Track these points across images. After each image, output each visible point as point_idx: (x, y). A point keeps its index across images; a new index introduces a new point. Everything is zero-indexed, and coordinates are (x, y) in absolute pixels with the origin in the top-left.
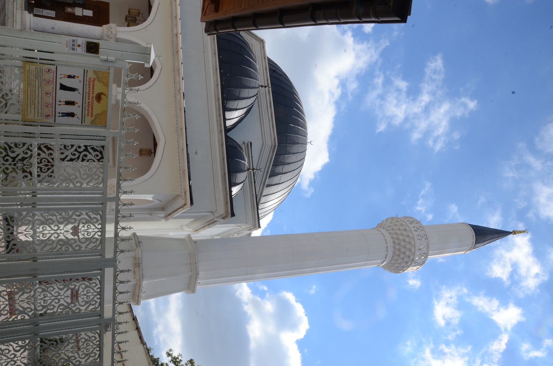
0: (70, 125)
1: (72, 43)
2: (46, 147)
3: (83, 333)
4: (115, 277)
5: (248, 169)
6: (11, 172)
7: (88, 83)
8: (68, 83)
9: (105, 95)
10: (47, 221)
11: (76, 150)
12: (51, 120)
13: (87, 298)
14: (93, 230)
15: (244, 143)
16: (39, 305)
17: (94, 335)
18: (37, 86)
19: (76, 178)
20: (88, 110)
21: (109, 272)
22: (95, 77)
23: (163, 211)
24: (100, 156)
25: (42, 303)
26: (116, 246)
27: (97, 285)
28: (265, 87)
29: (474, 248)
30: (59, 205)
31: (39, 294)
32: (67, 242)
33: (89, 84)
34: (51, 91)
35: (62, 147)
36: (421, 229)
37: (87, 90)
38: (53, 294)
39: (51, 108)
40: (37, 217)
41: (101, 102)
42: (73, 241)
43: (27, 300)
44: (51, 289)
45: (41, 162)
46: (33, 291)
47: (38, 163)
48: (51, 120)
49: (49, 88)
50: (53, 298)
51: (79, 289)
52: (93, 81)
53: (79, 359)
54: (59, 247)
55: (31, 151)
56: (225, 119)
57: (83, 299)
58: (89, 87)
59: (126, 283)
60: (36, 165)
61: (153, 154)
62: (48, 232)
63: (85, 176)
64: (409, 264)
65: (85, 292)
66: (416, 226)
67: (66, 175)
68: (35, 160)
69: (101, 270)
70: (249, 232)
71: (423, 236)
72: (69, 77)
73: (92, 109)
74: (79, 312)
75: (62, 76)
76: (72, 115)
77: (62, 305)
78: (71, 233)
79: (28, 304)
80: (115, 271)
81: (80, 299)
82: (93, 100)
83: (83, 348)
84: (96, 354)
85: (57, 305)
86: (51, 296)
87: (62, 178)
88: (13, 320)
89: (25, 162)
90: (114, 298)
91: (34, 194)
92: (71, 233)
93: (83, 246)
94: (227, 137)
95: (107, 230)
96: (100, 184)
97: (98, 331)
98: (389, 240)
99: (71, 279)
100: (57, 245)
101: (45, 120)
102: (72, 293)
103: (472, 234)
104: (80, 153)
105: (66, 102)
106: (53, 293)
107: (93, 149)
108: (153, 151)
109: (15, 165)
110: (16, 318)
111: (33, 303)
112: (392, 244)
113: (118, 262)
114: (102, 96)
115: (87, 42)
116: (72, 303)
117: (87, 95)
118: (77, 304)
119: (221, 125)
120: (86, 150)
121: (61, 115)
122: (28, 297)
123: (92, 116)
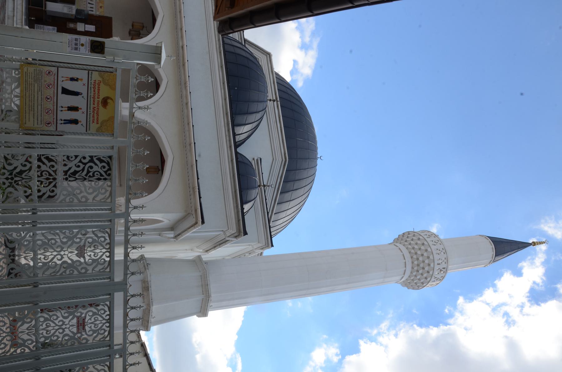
0: (74, 134)
1: (74, 42)
2: (47, 158)
3: (91, 366)
4: (126, 302)
5: (259, 186)
6: (9, 186)
7: (92, 86)
8: (71, 86)
9: (111, 99)
10: (49, 241)
11: (80, 161)
12: (52, 128)
13: (94, 327)
14: (101, 253)
15: (254, 159)
16: (41, 336)
17: (103, 368)
18: (36, 90)
19: (81, 192)
20: (93, 117)
21: (119, 297)
22: (101, 79)
23: (172, 230)
24: (107, 167)
25: (45, 334)
26: (126, 268)
27: (105, 311)
28: (274, 101)
29: (494, 262)
30: (62, 223)
31: (41, 323)
32: (73, 265)
33: (94, 88)
34: (52, 96)
35: (65, 158)
36: (440, 242)
37: (92, 94)
38: (57, 323)
39: (52, 115)
40: (38, 237)
41: (108, 107)
42: (78, 264)
43: (27, 331)
44: (55, 317)
45: (42, 175)
46: (34, 321)
47: (38, 176)
48: (52, 128)
49: (50, 92)
50: (57, 327)
51: (85, 317)
52: (99, 84)
53: (85, 194)
54: (62, 270)
55: (30, 163)
56: (234, 135)
57: (90, 327)
58: (94, 91)
59: (138, 309)
60: (36, 179)
61: (160, 171)
62: (51, 253)
63: (91, 333)
64: (428, 279)
65: (93, 320)
66: (434, 239)
67: (70, 189)
68: (34, 173)
69: (110, 294)
70: (261, 251)
71: (441, 250)
72: (72, 79)
73: (98, 115)
74: (86, 343)
75: (64, 79)
76: (75, 122)
77: (65, 262)
78: (76, 254)
79: (29, 335)
80: (125, 296)
81: (87, 328)
82: (98, 105)
83: (91, 251)
84: (106, 191)
85: (61, 336)
86: (54, 325)
87: (65, 193)
88: (12, 354)
89: (23, 176)
90: (125, 326)
91: (35, 211)
92: (76, 254)
93: (90, 268)
94: (237, 153)
95: (115, 252)
96: (107, 268)
97: (108, 230)
98: (407, 256)
99: (76, 306)
100: (60, 268)
101: (46, 128)
102: (78, 321)
103: (490, 248)
104: (85, 164)
105: (68, 107)
106: (56, 322)
107: (99, 159)
108: (160, 169)
109: (12, 179)
110: (15, 351)
111: (34, 334)
112: (410, 260)
113: (128, 285)
114: (109, 101)
115: (91, 41)
116: (78, 332)
117: (92, 99)
118: (83, 333)
119: (230, 141)
120: (92, 161)
121: (63, 122)
122: (29, 327)
123: (97, 123)
